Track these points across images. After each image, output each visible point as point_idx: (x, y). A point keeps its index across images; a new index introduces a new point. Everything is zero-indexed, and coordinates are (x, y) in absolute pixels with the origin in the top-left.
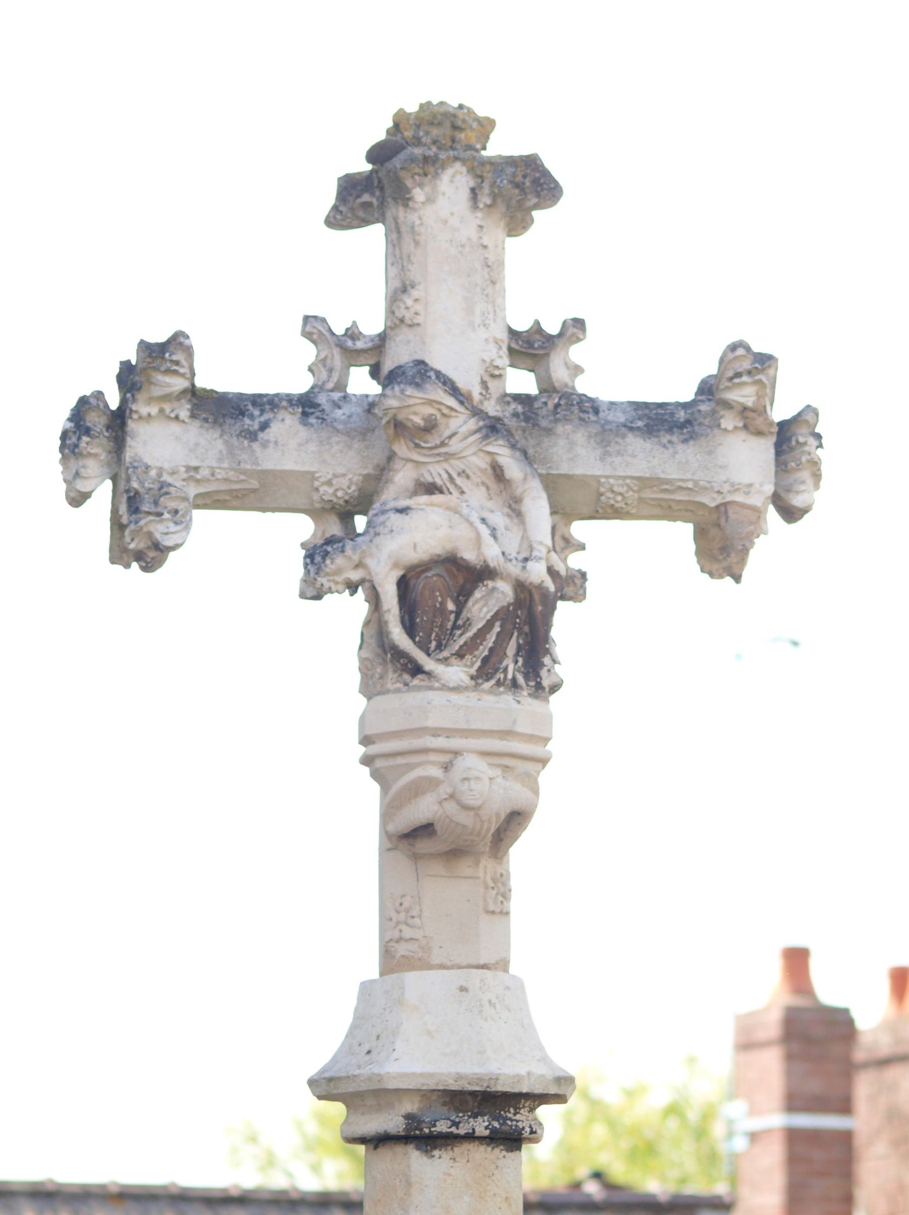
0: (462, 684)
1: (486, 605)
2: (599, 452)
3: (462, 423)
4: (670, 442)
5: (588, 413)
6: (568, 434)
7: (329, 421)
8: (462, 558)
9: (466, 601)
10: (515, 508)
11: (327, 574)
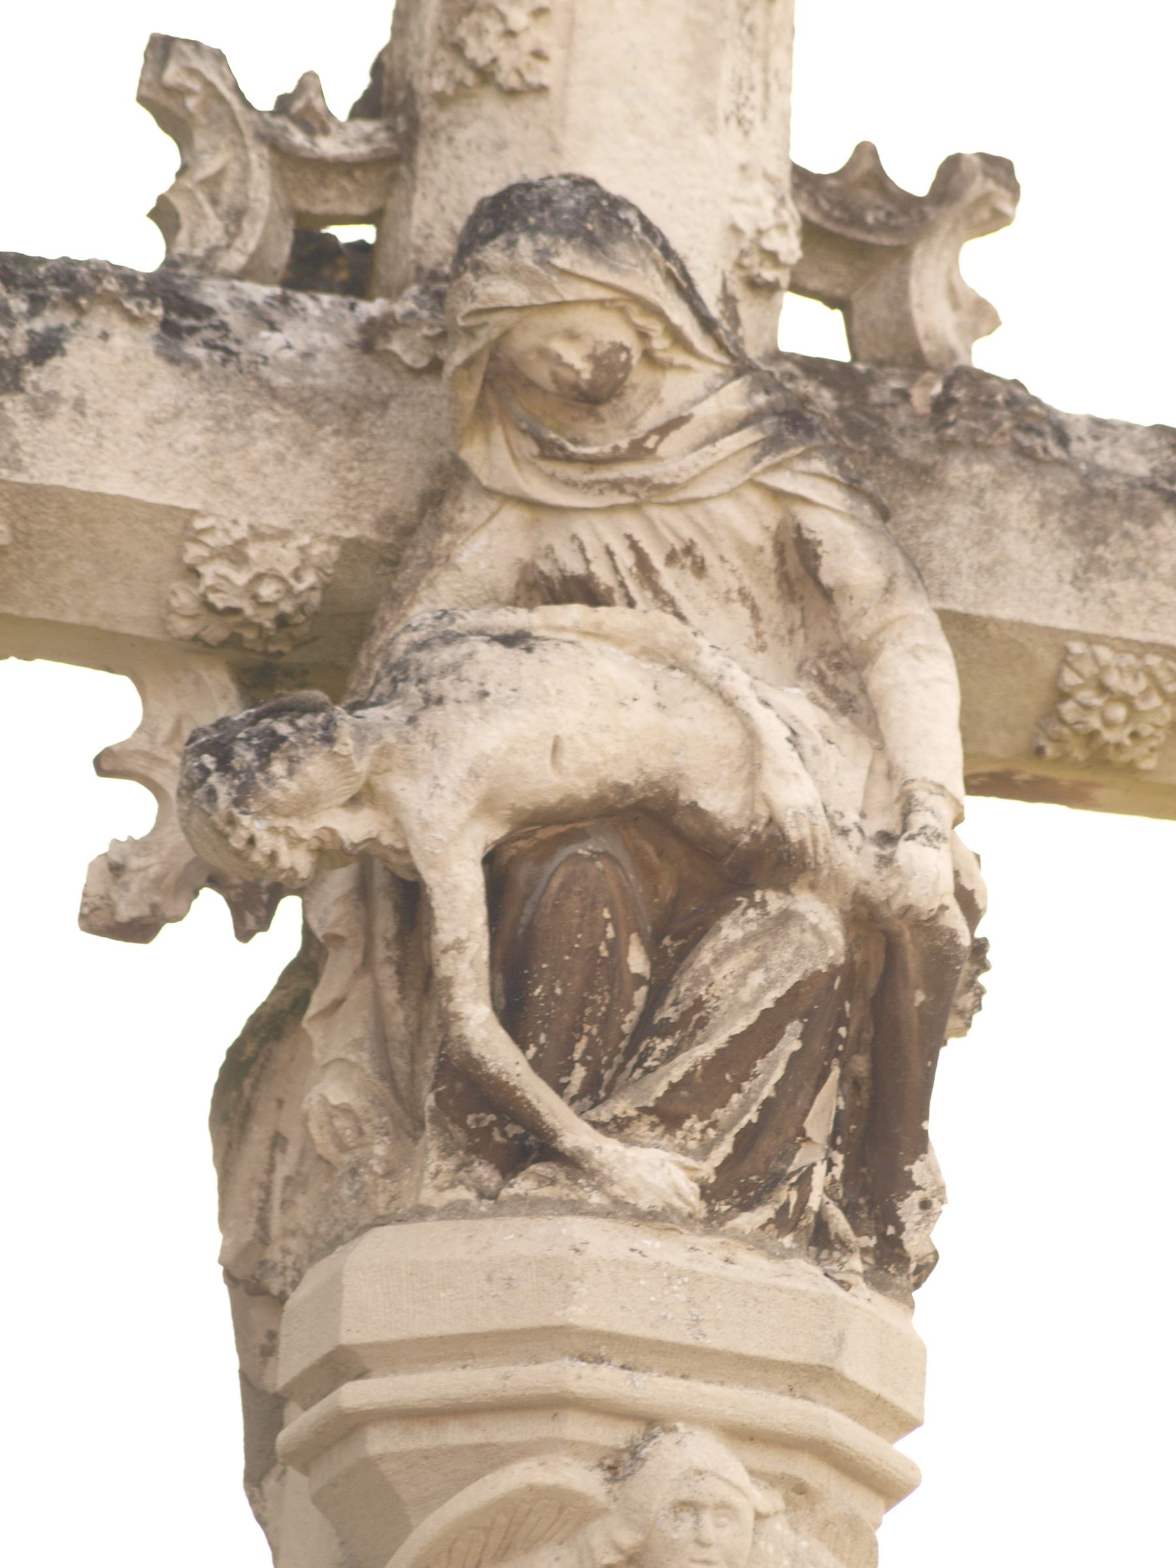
0: (678, 1203)
1: (761, 961)
2: (1071, 557)
3: (700, 391)
5: (1040, 434)
6: (982, 491)
7: (244, 357)
8: (693, 807)
10: (843, 679)
11: (272, 808)
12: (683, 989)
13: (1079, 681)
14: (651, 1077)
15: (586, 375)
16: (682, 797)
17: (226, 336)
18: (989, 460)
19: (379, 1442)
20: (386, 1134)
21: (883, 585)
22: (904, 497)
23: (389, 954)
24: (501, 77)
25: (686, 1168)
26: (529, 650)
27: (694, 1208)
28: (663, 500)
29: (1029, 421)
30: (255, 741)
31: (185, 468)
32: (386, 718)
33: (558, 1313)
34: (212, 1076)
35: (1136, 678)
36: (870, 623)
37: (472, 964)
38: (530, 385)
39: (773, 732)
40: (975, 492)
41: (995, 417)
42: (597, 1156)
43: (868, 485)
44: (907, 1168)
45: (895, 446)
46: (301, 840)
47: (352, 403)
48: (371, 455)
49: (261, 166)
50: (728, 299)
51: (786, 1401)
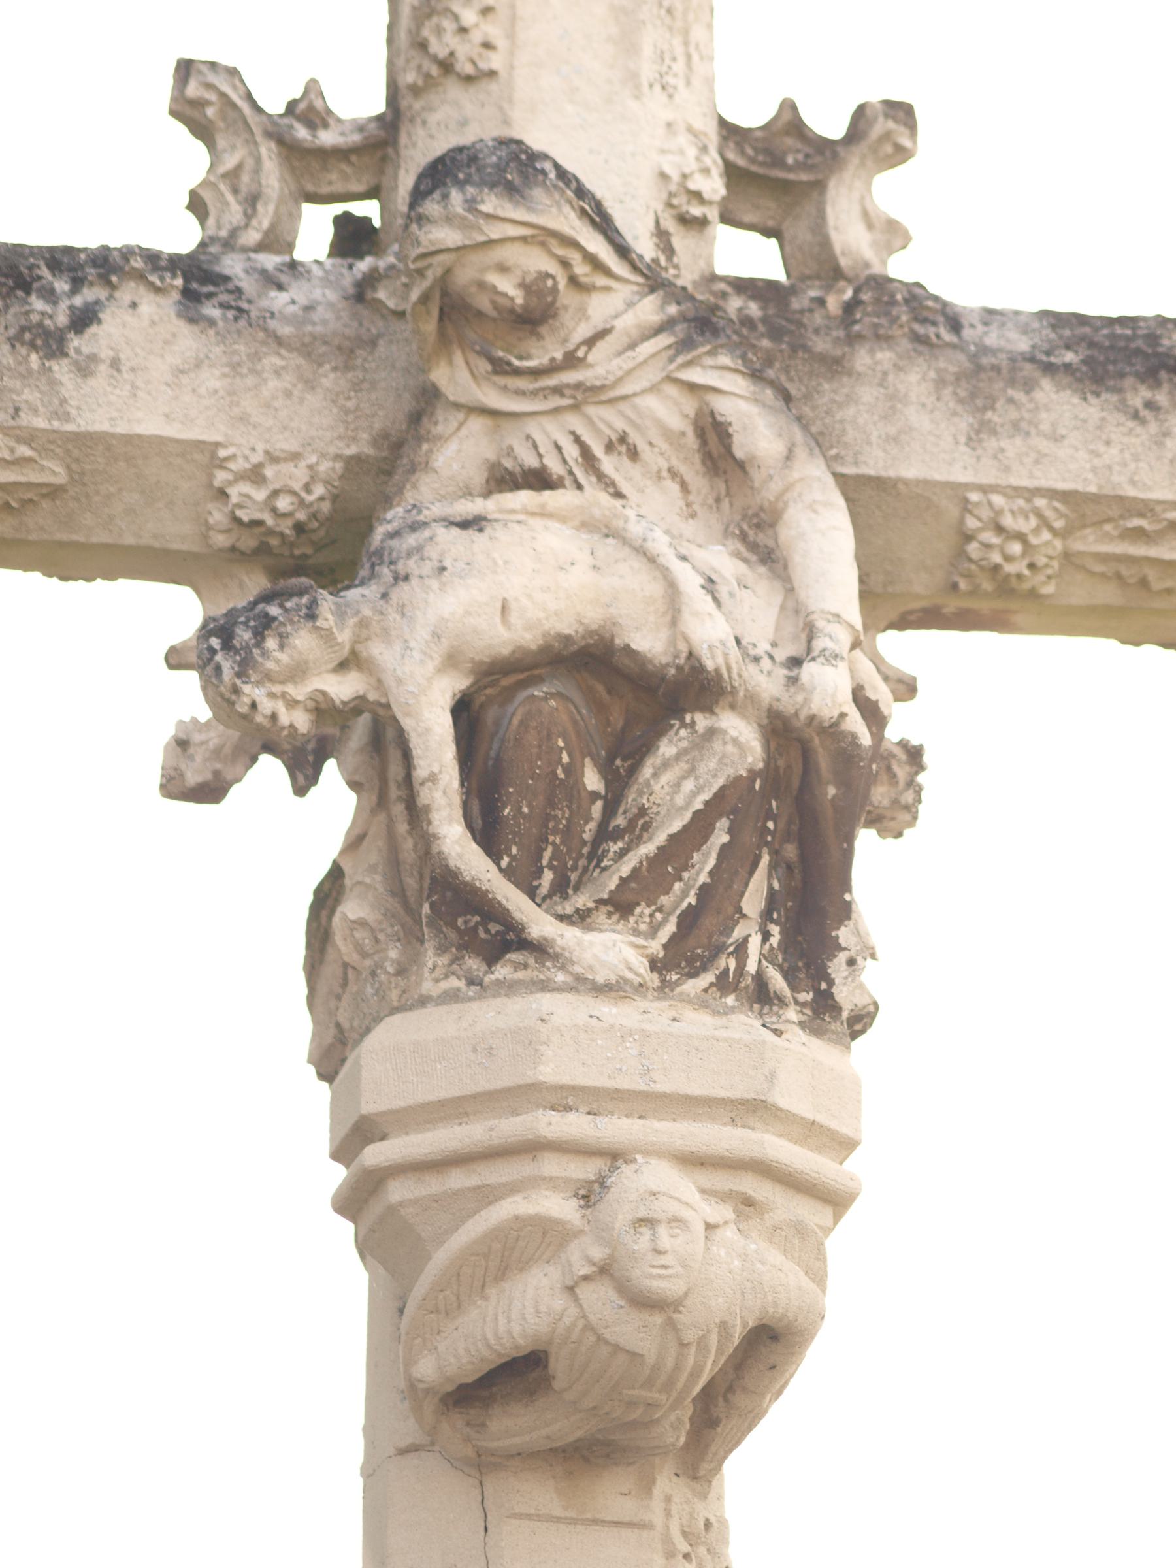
0: (629, 975)
2: (964, 423)
4: (1150, 405)
5: (934, 324)
6: (885, 374)
7: (254, 314)
8: (627, 648)
9: (633, 771)
10: (760, 539)
11: (268, 677)
12: (630, 800)
13: (979, 524)
14: (606, 873)
15: (519, 301)
16: (617, 641)
17: (240, 298)
18: (890, 348)
19: (398, 1191)
20: (399, 940)
21: (785, 454)
22: (819, 384)
23: (400, 793)
24: (458, 67)
25: (637, 947)
26: (481, 530)
27: (643, 978)
28: (597, 400)
29: (925, 314)
30: (252, 623)
31: (207, 408)
32: (363, 596)
33: (530, 1073)
34: (305, 913)
35: (1027, 518)
36: (775, 487)
37: (444, 793)
38: (480, 314)
39: (689, 581)
40: (879, 375)
41: (894, 313)
42: (559, 942)
43: (771, 373)
44: (833, 934)
45: (810, 343)
46: (297, 702)
47: (347, 343)
48: (365, 386)
49: (270, 157)
50: (662, 236)
51: (729, 1131)
